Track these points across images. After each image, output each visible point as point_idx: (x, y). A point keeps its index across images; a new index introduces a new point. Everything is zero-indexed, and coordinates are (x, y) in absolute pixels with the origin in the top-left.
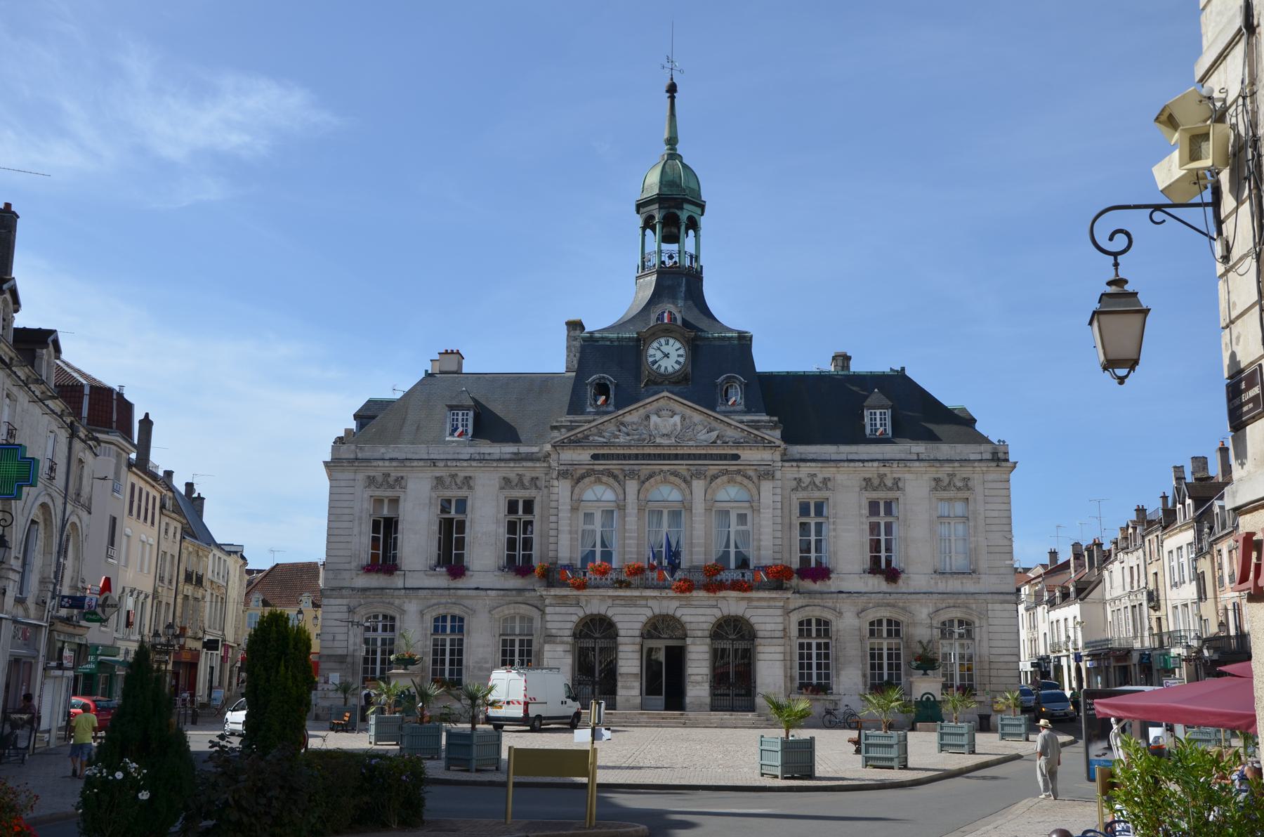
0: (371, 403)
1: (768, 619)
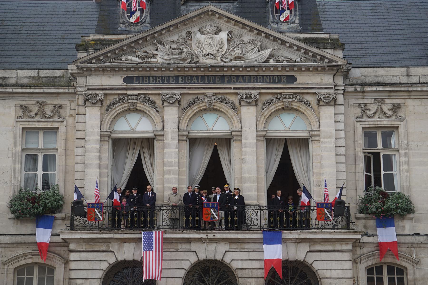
1: (334, 265)
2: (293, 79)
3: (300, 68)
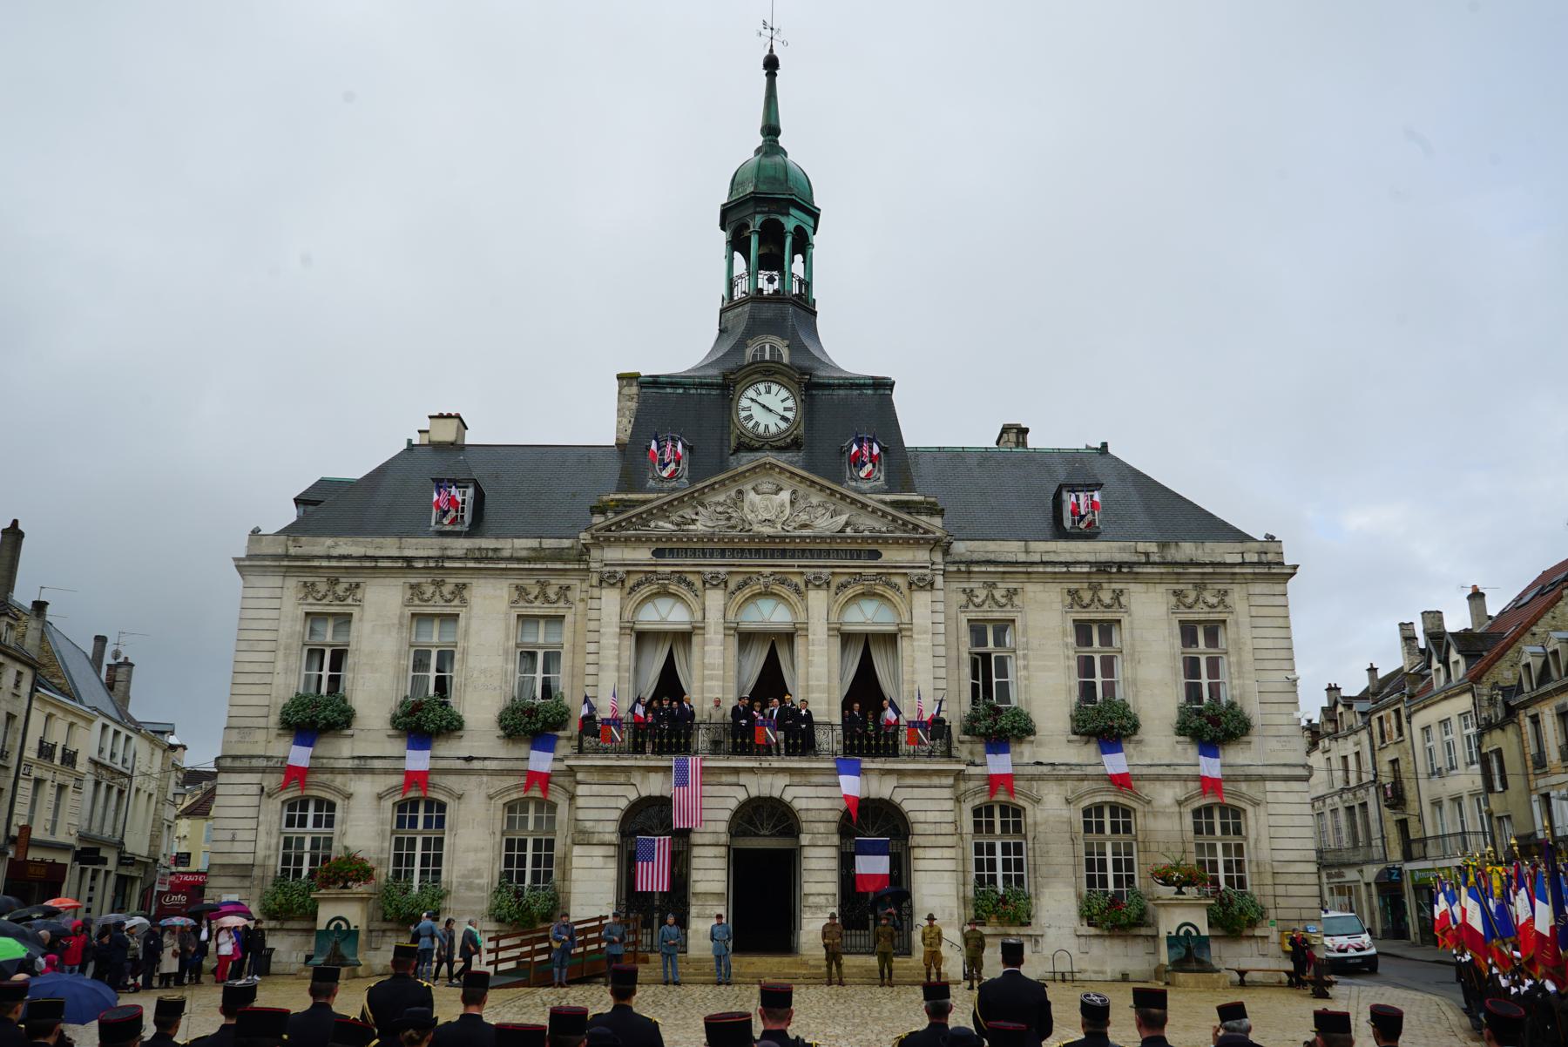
0: (323, 485)
1: (929, 805)
2: (876, 555)
3: (886, 541)
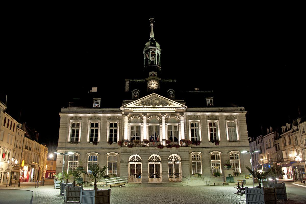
1: (185, 155)
